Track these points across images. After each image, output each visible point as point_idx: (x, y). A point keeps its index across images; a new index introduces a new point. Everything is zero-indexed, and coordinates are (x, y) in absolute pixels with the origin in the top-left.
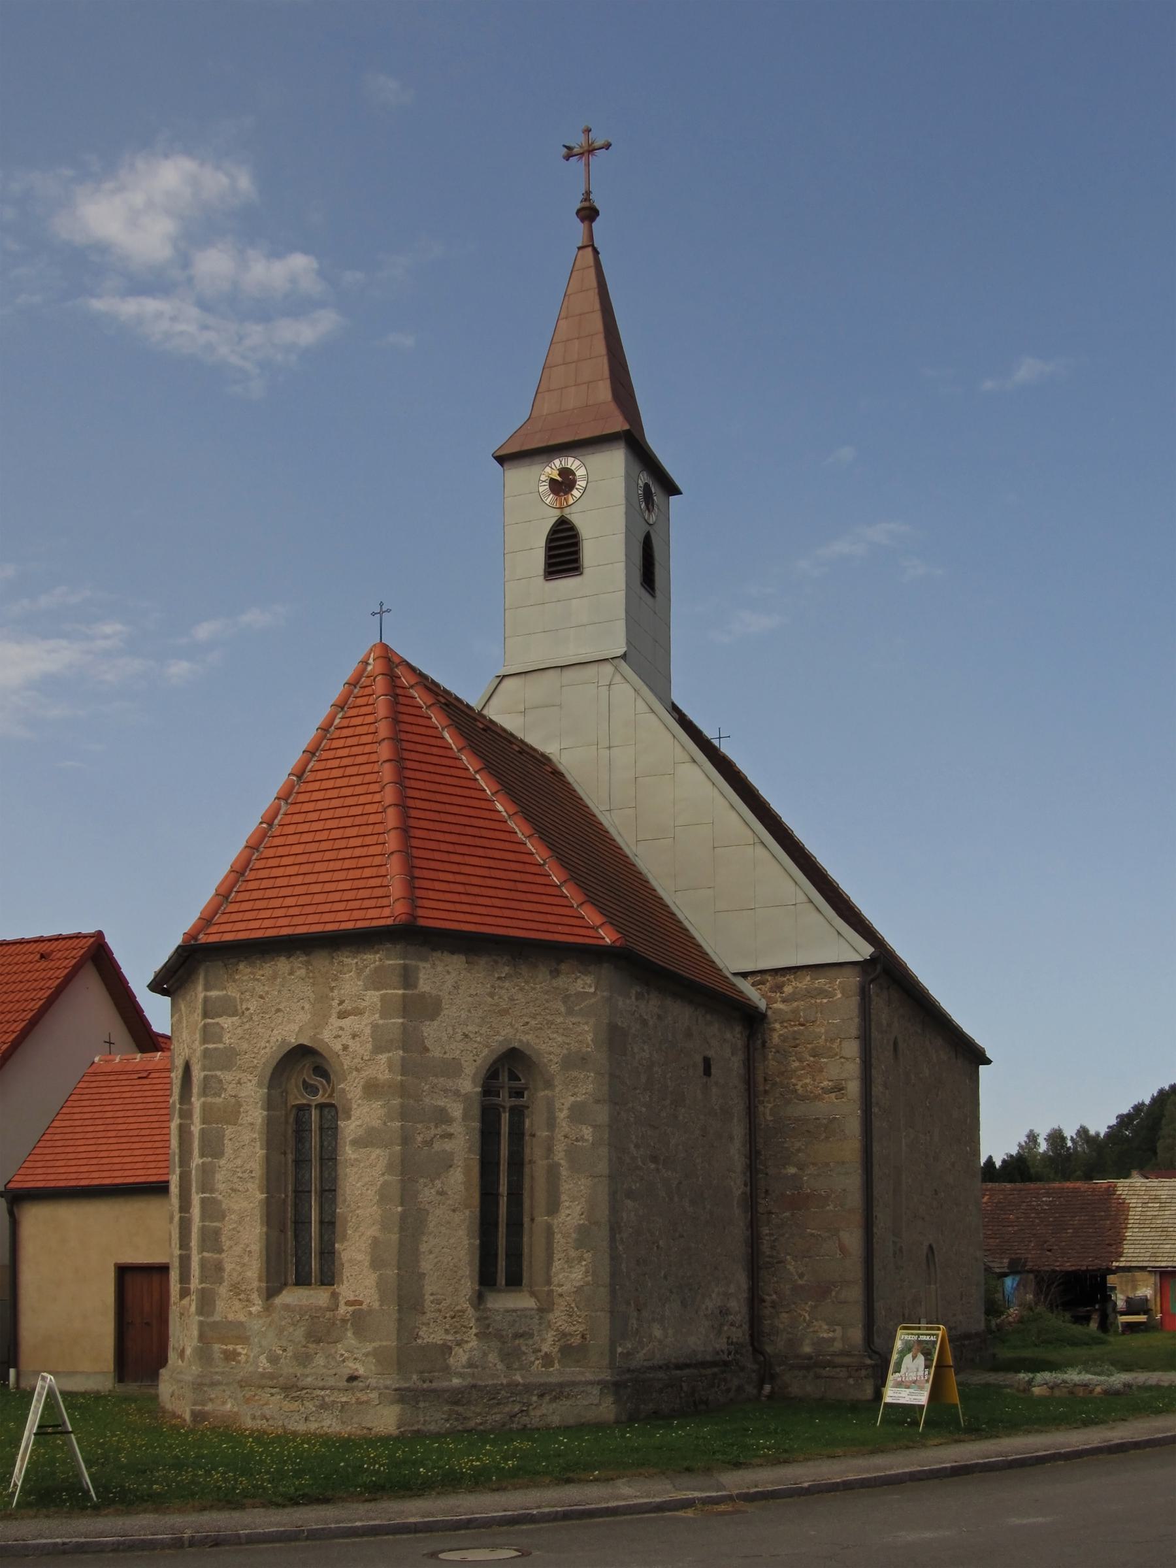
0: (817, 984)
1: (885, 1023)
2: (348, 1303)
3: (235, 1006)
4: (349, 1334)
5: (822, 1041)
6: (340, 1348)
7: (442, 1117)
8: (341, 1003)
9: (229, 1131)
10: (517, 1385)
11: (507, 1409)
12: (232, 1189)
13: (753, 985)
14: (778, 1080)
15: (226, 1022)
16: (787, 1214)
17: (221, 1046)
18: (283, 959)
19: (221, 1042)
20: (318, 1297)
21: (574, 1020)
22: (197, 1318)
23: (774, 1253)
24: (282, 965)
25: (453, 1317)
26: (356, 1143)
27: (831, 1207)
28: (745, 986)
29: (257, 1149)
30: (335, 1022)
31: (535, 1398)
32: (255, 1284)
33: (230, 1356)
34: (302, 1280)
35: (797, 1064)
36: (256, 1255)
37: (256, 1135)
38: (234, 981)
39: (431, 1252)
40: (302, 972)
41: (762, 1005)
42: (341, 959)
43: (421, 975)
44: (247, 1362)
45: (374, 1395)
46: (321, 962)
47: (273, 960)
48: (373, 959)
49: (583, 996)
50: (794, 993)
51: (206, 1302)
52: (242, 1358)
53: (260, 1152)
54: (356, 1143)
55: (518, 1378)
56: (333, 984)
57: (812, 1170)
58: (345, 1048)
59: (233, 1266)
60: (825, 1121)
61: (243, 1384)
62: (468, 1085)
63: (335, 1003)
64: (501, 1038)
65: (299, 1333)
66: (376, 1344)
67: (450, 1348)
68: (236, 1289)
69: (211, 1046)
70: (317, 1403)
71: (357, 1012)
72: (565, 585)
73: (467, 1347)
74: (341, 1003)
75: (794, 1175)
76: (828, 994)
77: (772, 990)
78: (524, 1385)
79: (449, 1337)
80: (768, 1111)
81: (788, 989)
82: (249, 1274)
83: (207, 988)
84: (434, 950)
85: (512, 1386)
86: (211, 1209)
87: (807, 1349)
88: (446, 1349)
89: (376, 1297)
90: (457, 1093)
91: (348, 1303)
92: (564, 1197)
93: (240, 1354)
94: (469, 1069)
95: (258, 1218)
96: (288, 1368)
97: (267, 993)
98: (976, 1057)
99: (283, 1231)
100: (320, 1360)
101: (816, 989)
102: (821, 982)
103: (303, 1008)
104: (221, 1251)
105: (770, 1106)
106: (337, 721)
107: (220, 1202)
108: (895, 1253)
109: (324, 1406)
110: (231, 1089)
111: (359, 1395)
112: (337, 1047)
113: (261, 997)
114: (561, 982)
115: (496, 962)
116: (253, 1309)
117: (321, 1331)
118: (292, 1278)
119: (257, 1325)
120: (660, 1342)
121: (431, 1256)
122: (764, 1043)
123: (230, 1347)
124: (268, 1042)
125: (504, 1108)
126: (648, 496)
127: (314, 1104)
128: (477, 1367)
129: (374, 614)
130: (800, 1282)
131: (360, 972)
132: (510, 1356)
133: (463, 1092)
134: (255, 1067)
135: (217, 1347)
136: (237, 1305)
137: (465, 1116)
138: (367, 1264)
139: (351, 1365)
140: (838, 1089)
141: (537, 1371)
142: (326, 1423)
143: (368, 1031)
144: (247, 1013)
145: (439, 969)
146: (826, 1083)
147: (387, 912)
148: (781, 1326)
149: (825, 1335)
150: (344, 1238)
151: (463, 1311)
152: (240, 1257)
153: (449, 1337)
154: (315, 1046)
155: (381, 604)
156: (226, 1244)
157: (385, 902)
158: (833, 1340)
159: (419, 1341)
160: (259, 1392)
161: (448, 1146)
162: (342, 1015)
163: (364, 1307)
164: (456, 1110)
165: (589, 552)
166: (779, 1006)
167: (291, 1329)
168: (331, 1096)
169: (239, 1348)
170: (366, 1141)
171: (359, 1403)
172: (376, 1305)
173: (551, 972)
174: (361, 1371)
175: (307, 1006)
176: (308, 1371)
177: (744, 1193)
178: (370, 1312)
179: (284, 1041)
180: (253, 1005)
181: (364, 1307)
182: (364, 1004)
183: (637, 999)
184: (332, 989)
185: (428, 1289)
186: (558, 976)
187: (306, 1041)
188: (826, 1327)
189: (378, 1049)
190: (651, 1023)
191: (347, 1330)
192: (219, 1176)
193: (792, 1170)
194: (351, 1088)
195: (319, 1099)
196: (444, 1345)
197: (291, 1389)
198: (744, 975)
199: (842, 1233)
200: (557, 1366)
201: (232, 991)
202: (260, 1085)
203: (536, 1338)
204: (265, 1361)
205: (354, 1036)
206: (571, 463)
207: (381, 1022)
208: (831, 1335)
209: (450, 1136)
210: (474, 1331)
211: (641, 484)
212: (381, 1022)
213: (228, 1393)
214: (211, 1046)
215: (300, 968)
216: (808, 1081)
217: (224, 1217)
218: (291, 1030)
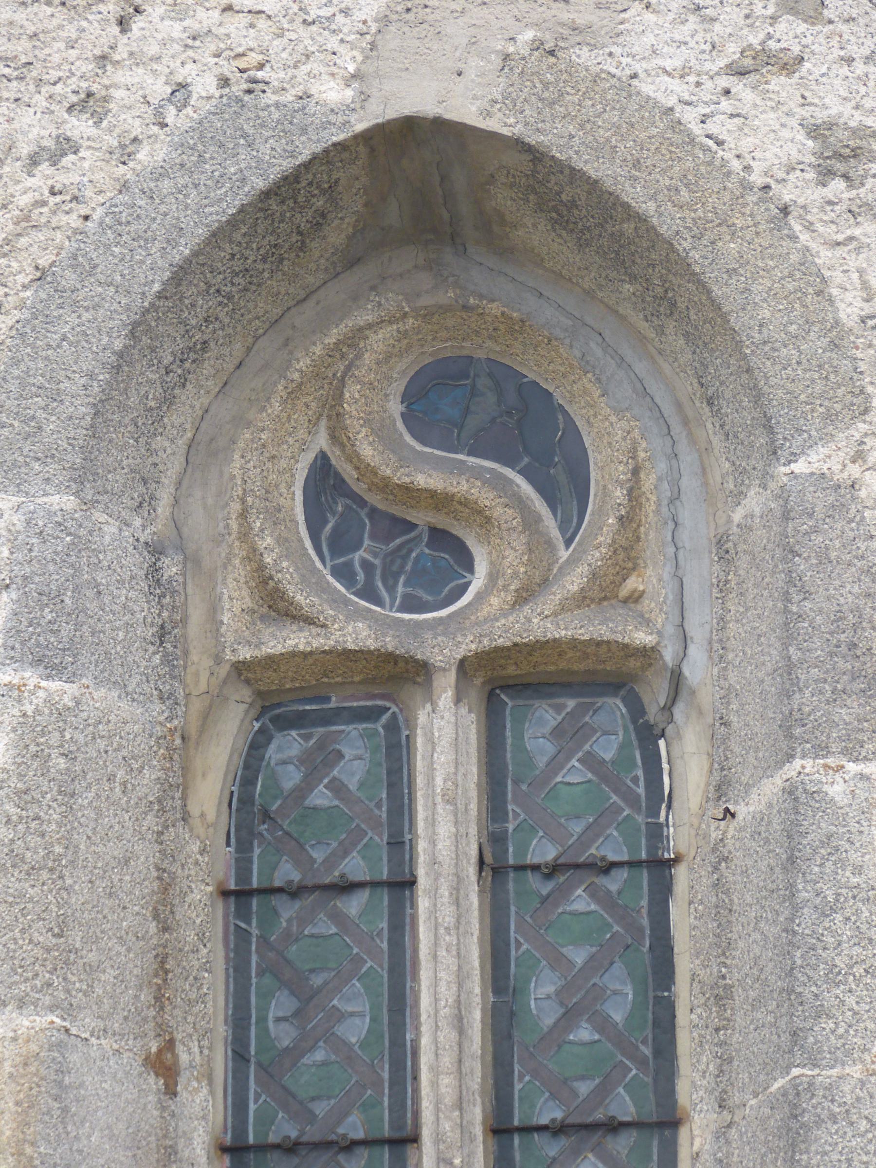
124: (88, 103)
127: (444, 652)
168: (607, 590)
187: (467, 100)
195: (493, 606)
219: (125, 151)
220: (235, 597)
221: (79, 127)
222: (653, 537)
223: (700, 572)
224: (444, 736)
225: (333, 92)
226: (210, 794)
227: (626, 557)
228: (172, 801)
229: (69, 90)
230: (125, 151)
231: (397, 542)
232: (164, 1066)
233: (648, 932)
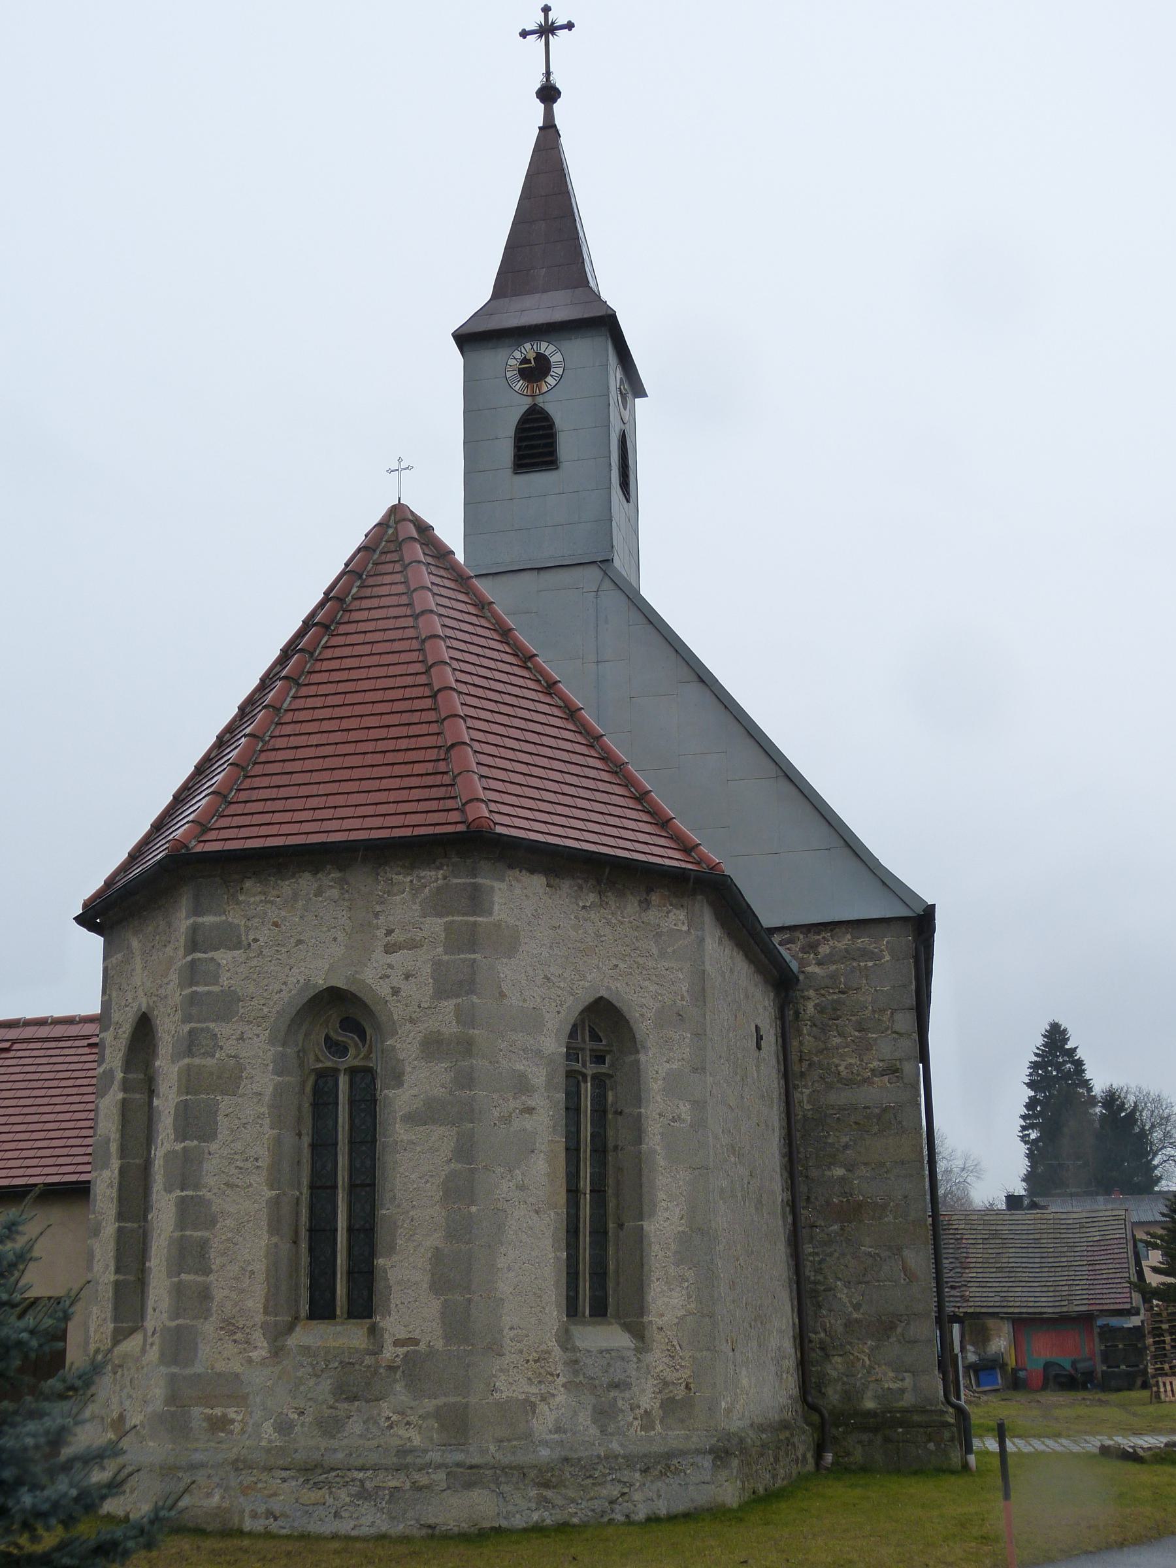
2: (397, 1343)
3: (239, 936)
4: (398, 1387)
5: (868, 1013)
6: (386, 1408)
7: (522, 1085)
8: (389, 932)
9: (225, 1103)
10: (616, 1457)
12: (227, 1184)
14: (816, 1059)
15: (224, 957)
16: (836, 1227)
17: (216, 989)
18: (307, 875)
19: (216, 983)
20: (348, 1336)
22: (163, 1370)
23: (820, 1278)
24: (306, 883)
25: (536, 1361)
26: (412, 1119)
27: (890, 1218)
29: (266, 1128)
30: (379, 957)
31: (637, 1475)
32: (259, 1318)
33: (218, 1425)
34: (321, 1310)
36: (261, 1277)
37: (264, 1110)
38: (238, 903)
39: (509, 1269)
40: (335, 893)
42: (389, 875)
43: (496, 899)
44: (243, 1432)
45: (441, 1476)
46: (361, 880)
47: (293, 876)
48: (433, 877)
50: (831, 955)
51: (179, 1346)
53: (269, 1133)
54: (412, 1119)
55: (615, 1446)
56: (378, 908)
57: (863, 1171)
58: (395, 992)
59: (226, 1292)
60: (877, 1111)
61: (239, 1465)
62: (553, 1045)
63: (381, 933)
64: (587, 985)
65: (326, 1385)
66: (441, 1401)
67: (533, 1405)
69: (200, 989)
70: (354, 1490)
71: (413, 945)
72: (539, 480)
74: (389, 932)
75: (842, 1179)
76: (871, 956)
77: (803, 950)
78: (624, 1457)
79: (533, 1390)
81: (824, 950)
82: (250, 1304)
83: (197, 911)
84: (511, 867)
85: (611, 1457)
86: (192, 1213)
87: (870, 1404)
88: (529, 1406)
89: (440, 1333)
90: (538, 1053)
91: (397, 1343)
92: (661, 1195)
93: (232, 1421)
95: (264, 1224)
96: (308, 1442)
100: (355, 1426)
101: (859, 949)
102: (863, 941)
103: (335, 939)
104: (207, 1271)
105: (807, 1091)
106: (354, 590)
107: (209, 1202)
109: (364, 1495)
111: (416, 1476)
112: (384, 990)
113: (276, 924)
114: (652, 915)
115: (581, 888)
116: (254, 1355)
117: (355, 1386)
118: (305, 1309)
121: (510, 1275)
122: (797, 1013)
123: (218, 1411)
124: (285, 983)
125: (584, 1076)
127: (342, 1067)
128: (565, 1432)
129: (390, 471)
130: (855, 1315)
131: (415, 892)
132: (604, 1415)
134: (265, 1017)
135: (197, 1411)
136: (230, 1349)
138: (425, 1286)
139: (400, 1432)
141: (631, 1437)
142: (366, 1520)
143: (427, 969)
144: (254, 946)
145: (517, 891)
146: (875, 1064)
147: (455, 816)
148: (834, 1374)
149: (892, 1386)
150: (392, 1249)
151: (548, 1352)
152: (236, 1279)
153: (533, 1390)
154: (353, 989)
155: (400, 460)
156: (216, 1261)
157: (450, 804)
158: (902, 1391)
159: (497, 1396)
160: (264, 1476)
161: (528, 1123)
162: (390, 949)
163: (422, 1347)
164: (538, 1075)
165: (567, 446)
166: (812, 969)
167: (311, 1383)
168: (367, 1057)
170: (428, 1114)
171: (417, 1488)
172: (439, 1344)
174: (417, 1441)
175: (341, 937)
176: (334, 1443)
178: (431, 1353)
179: (307, 982)
180: (264, 935)
181: (422, 1347)
184: (376, 915)
185: (507, 1321)
186: (648, 908)
187: (340, 984)
188: (891, 1374)
189: (440, 993)
191: (395, 1381)
192: (209, 1166)
193: (839, 1172)
194: (404, 1045)
195: (351, 1060)
196: (526, 1400)
197: (312, 1471)
199: (906, 1253)
200: (658, 1427)
201: (234, 916)
202: (272, 1041)
203: (635, 1389)
204: (271, 1430)
206: (546, 348)
207: (446, 958)
208: (898, 1385)
209: (530, 1110)
210: (562, 1380)
212: (446, 958)
213: (216, 1479)
214: (200, 989)
215: (331, 887)
216: (853, 1061)
217: (213, 1222)
218: (320, 967)
219: (290, 991)
220: (312, 1057)
221: (284, 987)
222: (374, 1049)
223: (379, 1054)
224: (343, 1082)
225: (321, 982)
226: (309, 1088)
227: (370, 1052)
228: (302, 1091)
229: (831, 943)
230: (290, 991)
231: (337, 1048)
232: (299, 1135)
233: (450, 918)
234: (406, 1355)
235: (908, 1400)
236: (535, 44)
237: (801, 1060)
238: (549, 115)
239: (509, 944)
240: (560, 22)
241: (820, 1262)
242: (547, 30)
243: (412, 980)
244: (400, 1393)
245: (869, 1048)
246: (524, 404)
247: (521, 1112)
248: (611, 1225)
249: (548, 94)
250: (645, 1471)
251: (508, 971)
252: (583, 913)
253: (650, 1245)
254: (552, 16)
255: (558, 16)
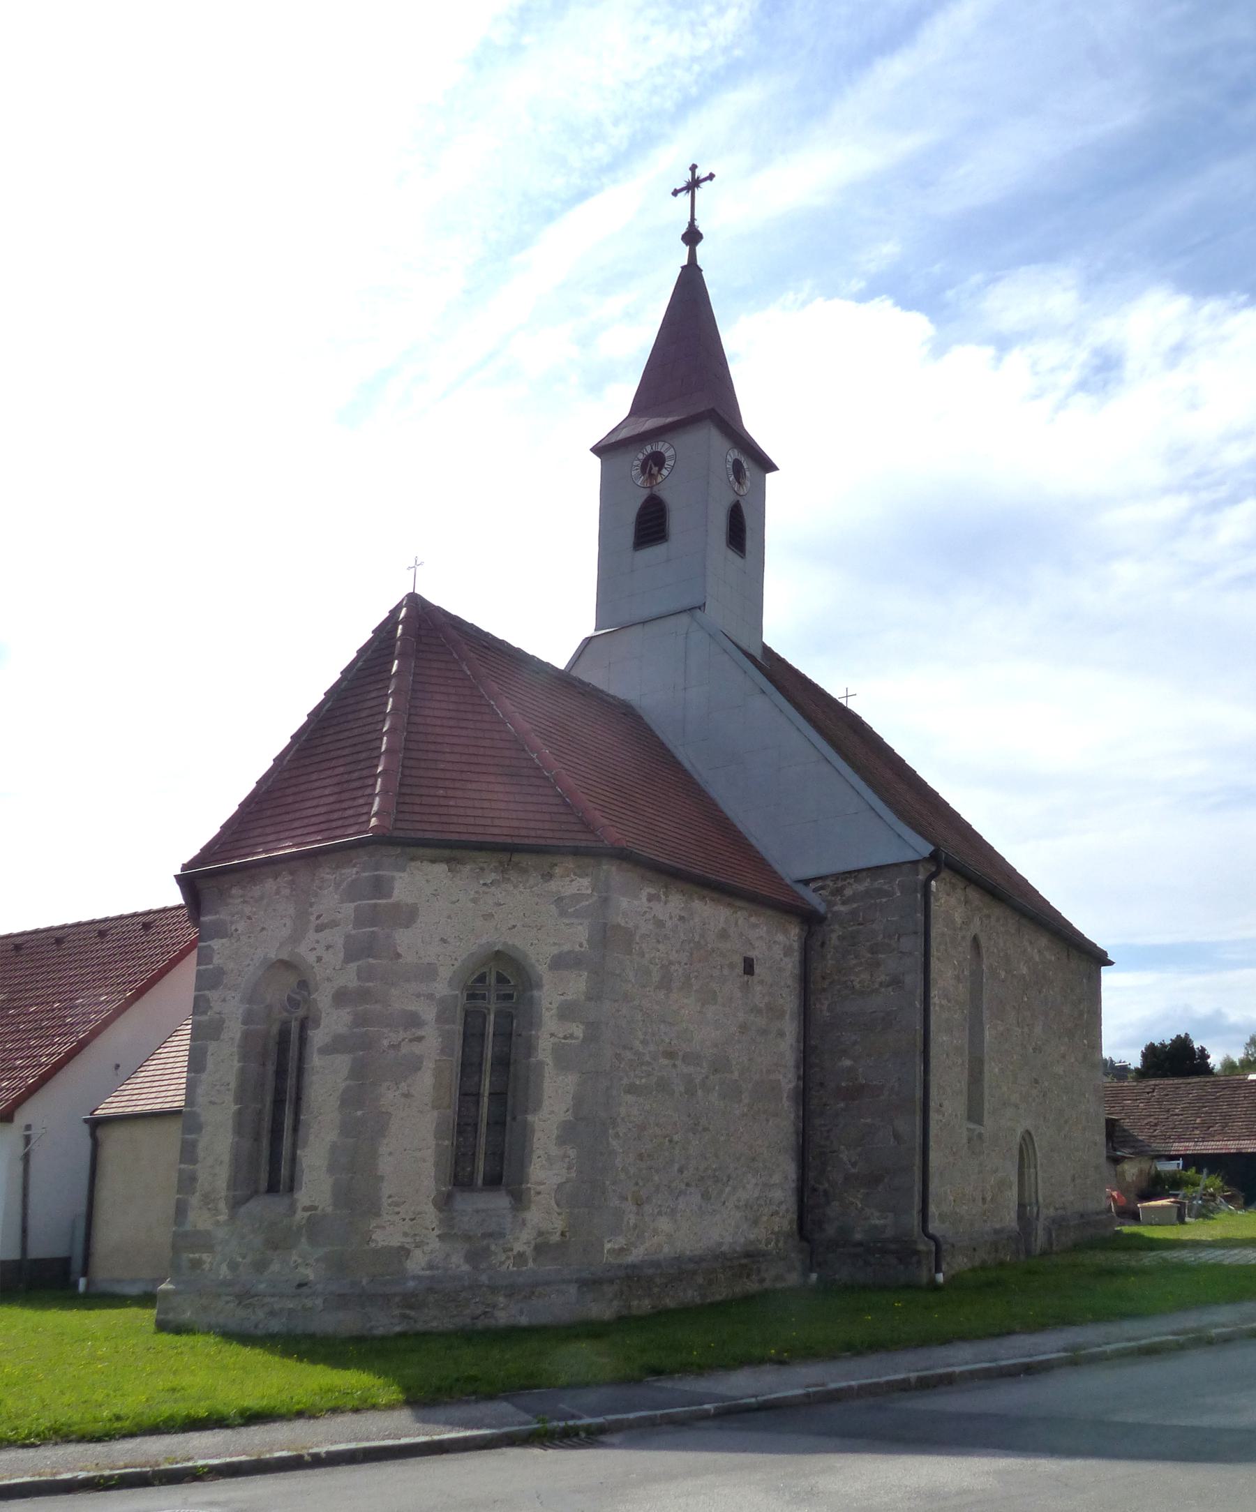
0: (876, 885)
1: (958, 920)
2: (305, 1209)
4: (303, 1240)
5: (880, 938)
8: (318, 917)
11: (467, 1312)
13: (815, 890)
15: (216, 944)
21: (567, 921)
26: (325, 1051)
28: (800, 889)
29: (236, 1062)
30: (311, 935)
33: (196, 1264)
35: (854, 962)
41: (822, 908)
44: (211, 1270)
45: (319, 1302)
49: (577, 898)
52: (206, 1266)
53: (237, 1065)
54: (325, 1051)
58: (319, 959)
63: (313, 918)
68: (207, 1199)
71: (334, 924)
73: (427, 1248)
80: (825, 1007)
81: (848, 892)
87: (858, 1236)
94: (445, 973)
97: (255, 913)
98: (1095, 958)
99: (257, 1139)
100: (275, 1267)
108: (970, 1140)
110: (216, 1006)
112: (311, 958)
113: (249, 918)
117: (278, 1240)
118: (264, 1185)
119: (221, 1233)
120: (669, 1236)
123: (197, 1255)
126: (738, 469)
128: (438, 1268)
130: (853, 1170)
132: (475, 1256)
133: (438, 996)
137: (440, 1019)
140: (896, 982)
149: (877, 1222)
152: (212, 1167)
153: (409, 1240)
156: (201, 1154)
158: (885, 1226)
161: (417, 1049)
162: (319, 929)
163: (318, 1212)
164: (429, 1013)
166: (839, 908)
169: (205, 1256)
170: (337, 1045)
172: (329, 1209)
173: (543, 875)
174: (312, 1277)
177: (797, 1087)
180: (241, 926)
181: (318, 1212)
182: (340, 916)
183: (649, 900)
184: (311, 905)
189: (349, 958)
190: (669, 924)
193: (847, 1063)
196: (402, 1248)
198: (806, 882)
200: (531, 1264)
205: (328, 947)
206: (661, 447)
207: (353, 932)
210: (437, 1232)
211: (730, 459)
234: (309, 1218)
235: (889, 1233)
236: (685, 198)
237: (824, 978)
238: (692, 256)
239: (406, 916)
240: (702, 177)
241: (828, 1131)
242: (693, 185)
243: (331, 950)
244: (304, 1243)
245: (878, 964)
246: (644, 494)
247: (411, 1041)
248: (508, 1118)
249: (692, 237)
250: (509, 1296)
251: (404, 939)
252: (484, 888)
253: (533, 1131)
254: (698, 172)
255: (701, 173)
